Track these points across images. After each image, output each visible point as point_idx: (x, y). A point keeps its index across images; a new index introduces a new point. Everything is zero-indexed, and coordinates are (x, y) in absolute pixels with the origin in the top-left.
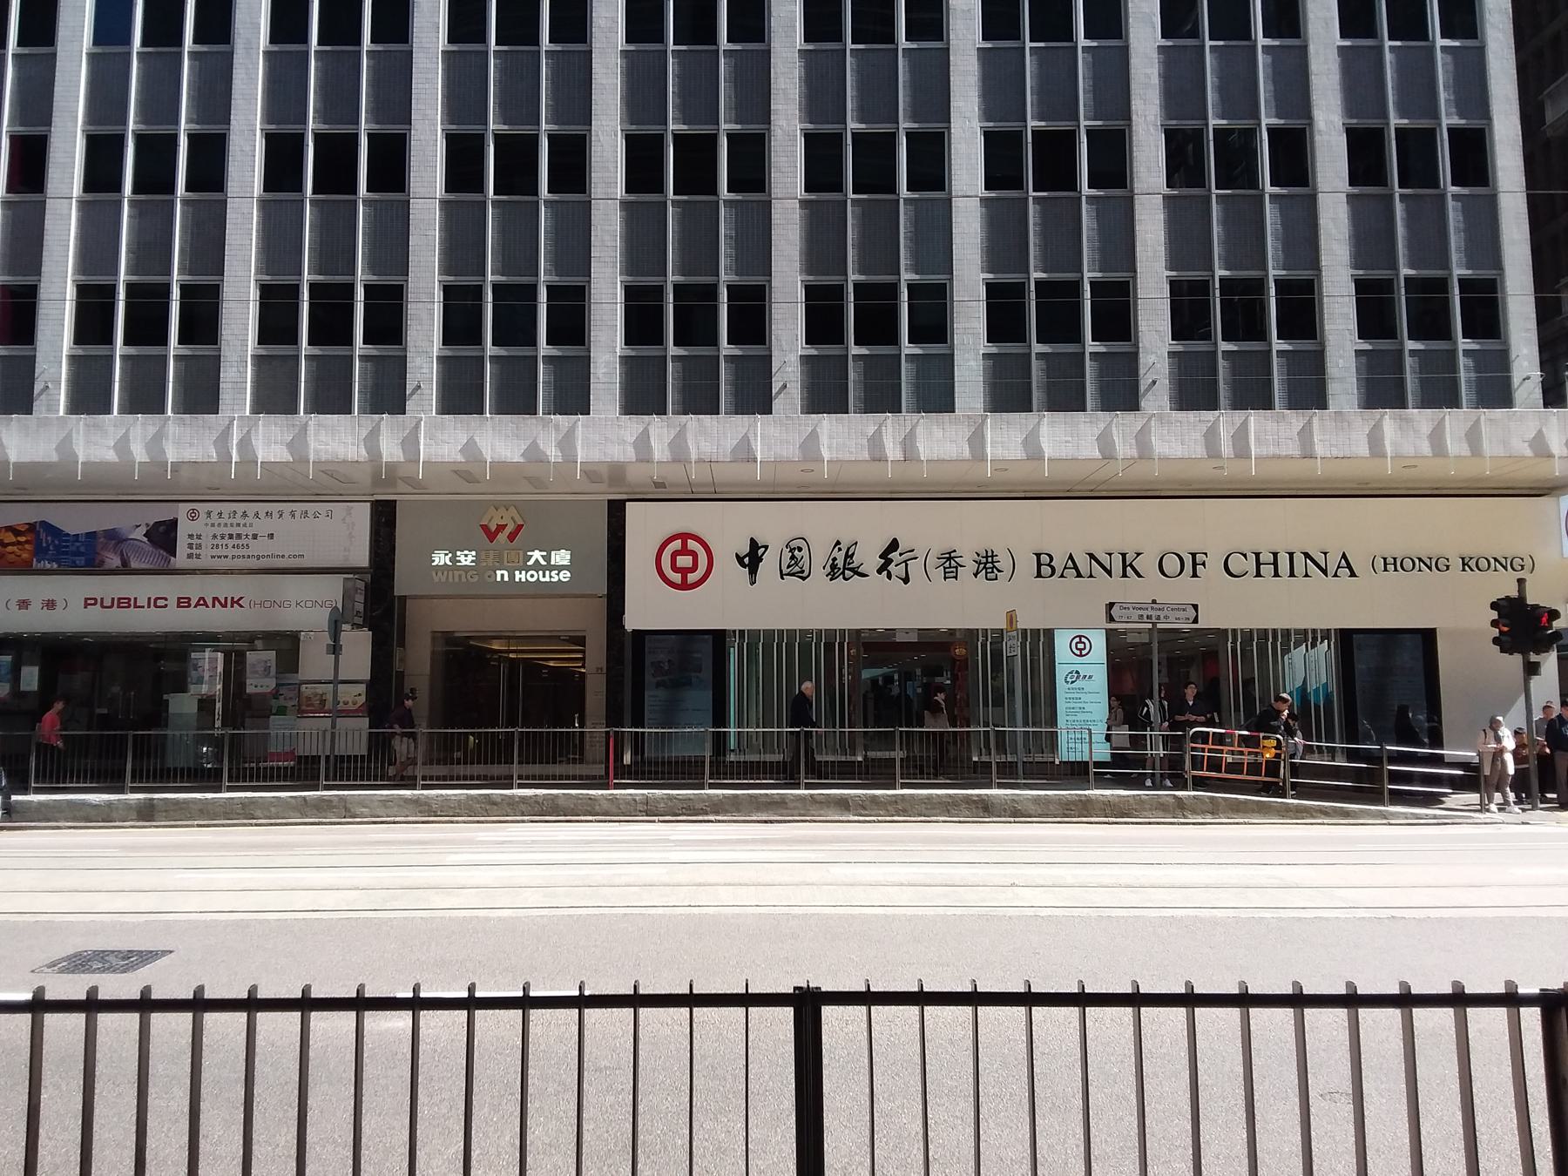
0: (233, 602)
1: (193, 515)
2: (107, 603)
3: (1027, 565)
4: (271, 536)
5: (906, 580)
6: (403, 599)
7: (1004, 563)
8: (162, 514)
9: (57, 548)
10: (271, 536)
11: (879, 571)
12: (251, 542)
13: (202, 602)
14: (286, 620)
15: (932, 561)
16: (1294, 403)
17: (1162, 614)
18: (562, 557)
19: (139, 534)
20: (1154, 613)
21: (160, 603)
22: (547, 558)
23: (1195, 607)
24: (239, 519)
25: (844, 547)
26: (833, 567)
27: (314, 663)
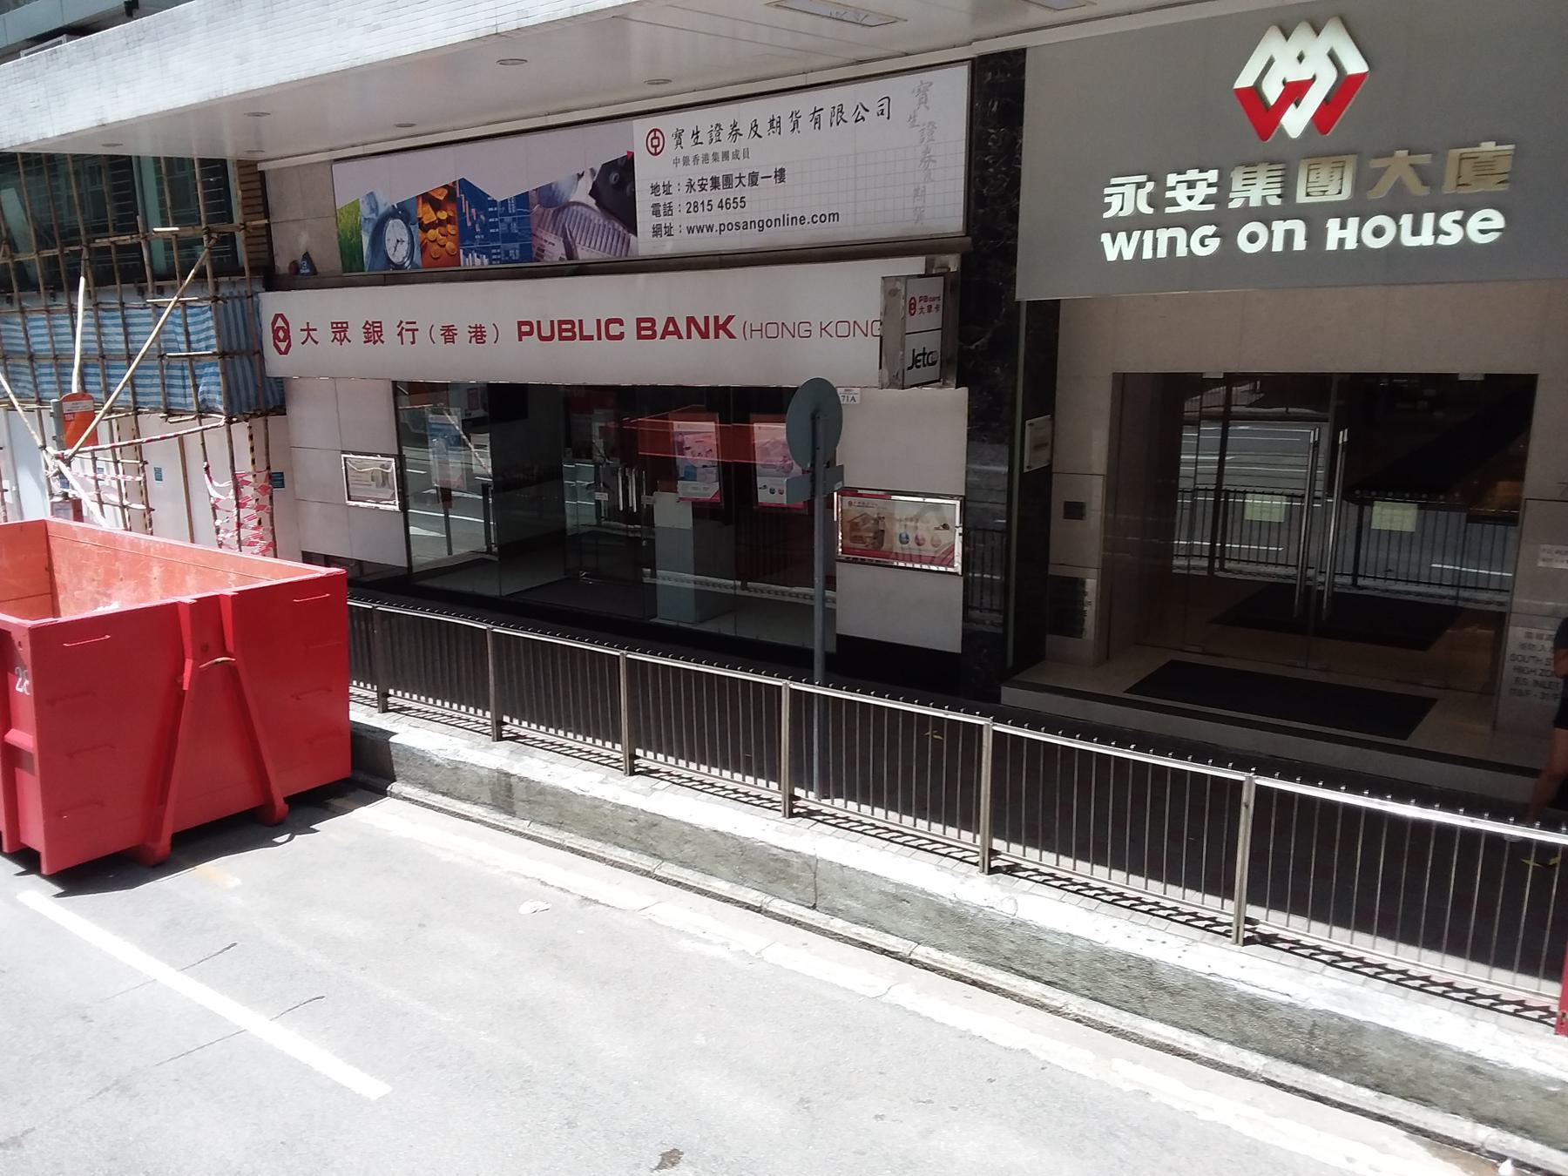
0: (718, 327)
1: (655, 144)
2: (546, 332)
4: (780, 175)
6: (1048, 312)
8: (603, 147)
9: (485, 227)
10: (780, 175)
12: (747, 192)
14: (785, 367)
19: (581, 193)
24: (726, 144)
27: (864, 454)
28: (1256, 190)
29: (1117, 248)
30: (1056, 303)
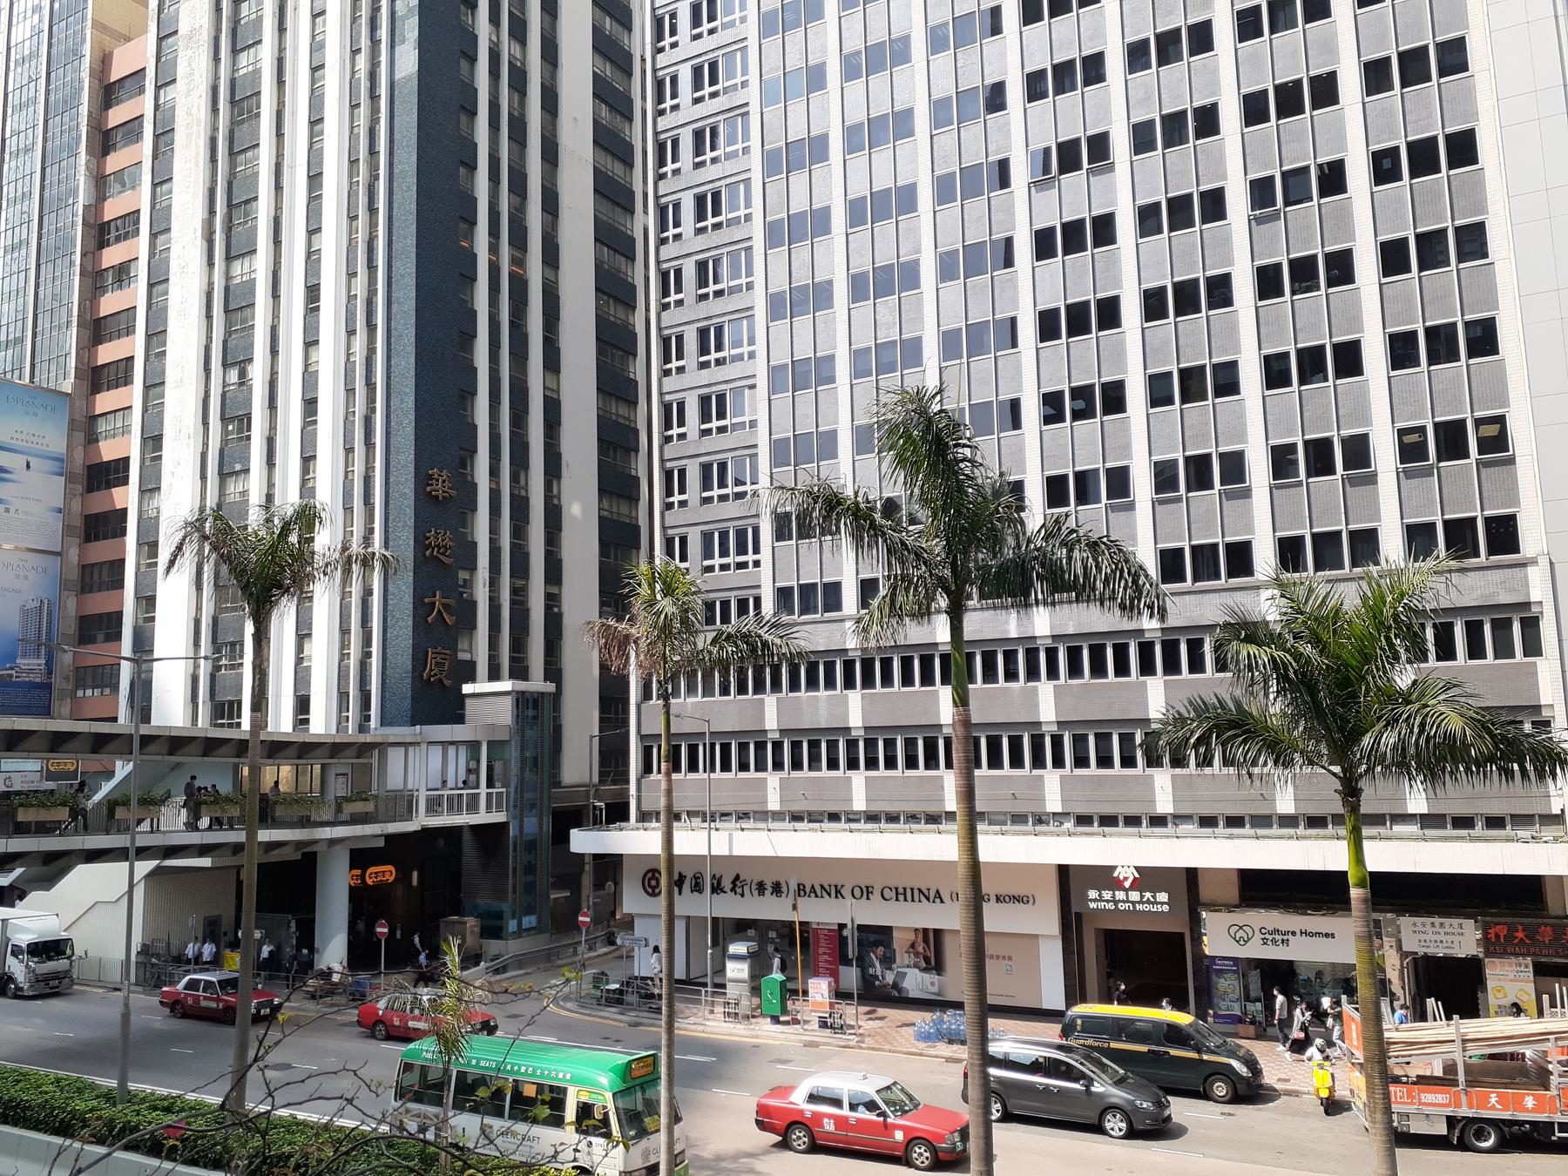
7: (784, 889)
18: (1163, 897)
28: (1120, 895)
29: (1092, 905)
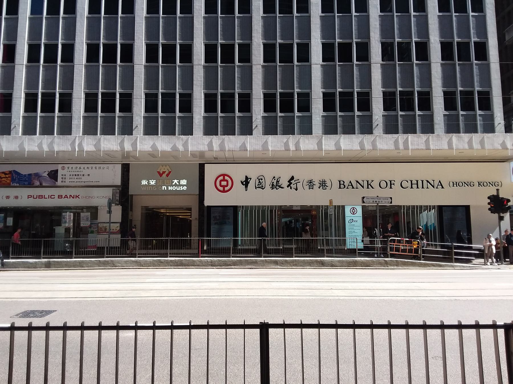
0: (76, 197)
1: (63, 168)
2: (35, 197)
3: (336, 184)
4: (89, 175)
5: (296, 189)
6: (132, 196)
7: (328, 184)
8: (53, 168)
9: (19, 179)
10: (89, 175)
11: (288, 187)
12: (82, 177)
13: (66, 196)
14: (94, 202)
15: (305, 183)
16: (424, 132)
17: (380, 201)
18: (184, 182)
19: (45, 174)
20: (377, 200)
21: (52, 197)
22: (179, 182)
23: (391, 198)
24: (78, 170)
25: (276, 178)
26: (273, 185)
27: (103, 217)
30: (506, 132)
